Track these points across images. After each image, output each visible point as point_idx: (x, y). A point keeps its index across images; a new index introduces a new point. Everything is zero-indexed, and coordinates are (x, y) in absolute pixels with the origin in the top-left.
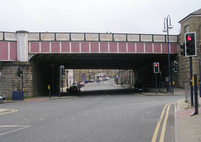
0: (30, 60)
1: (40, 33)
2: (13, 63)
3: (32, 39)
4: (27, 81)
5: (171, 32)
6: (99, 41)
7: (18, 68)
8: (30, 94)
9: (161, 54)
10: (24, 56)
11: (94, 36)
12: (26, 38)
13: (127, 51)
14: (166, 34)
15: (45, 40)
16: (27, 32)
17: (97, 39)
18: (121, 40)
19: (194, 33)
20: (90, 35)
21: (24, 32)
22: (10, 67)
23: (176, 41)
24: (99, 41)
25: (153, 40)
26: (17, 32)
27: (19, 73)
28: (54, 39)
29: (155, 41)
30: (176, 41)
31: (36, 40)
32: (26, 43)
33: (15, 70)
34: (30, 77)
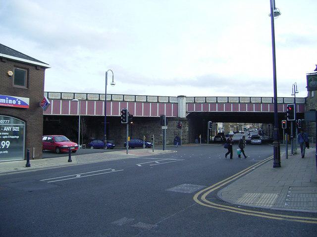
0: (187, 117)
1: (195, 97)
2: (175, 119)
3: (189, 102)
4: (184, 131)
5: (297, 96)
6: (239, 102)
7: (178, 122)
8: (187, 141)
9: (237, 112)
10: (183, 114)
11: (235, 99)
12: (184, 101)
13: (61, 112)
14: (294, 97)
15: (242, 102)
16: (185, 97)
17: (85, 99)
18: (257, 102)
19: (15, 84)
20: (232, 98)
21: (183, 96)
22: (173, 121)
23: (304, 102)
24: (239, 102)
25: (86, 100)
26: (178, 97)
27: (179, 127)
28: (205, 102)
29: (263, 102)
30: (304, 102)
31: (192, 102)
32: (185, 104)
33: (176, 123)
34: (187, 128)
